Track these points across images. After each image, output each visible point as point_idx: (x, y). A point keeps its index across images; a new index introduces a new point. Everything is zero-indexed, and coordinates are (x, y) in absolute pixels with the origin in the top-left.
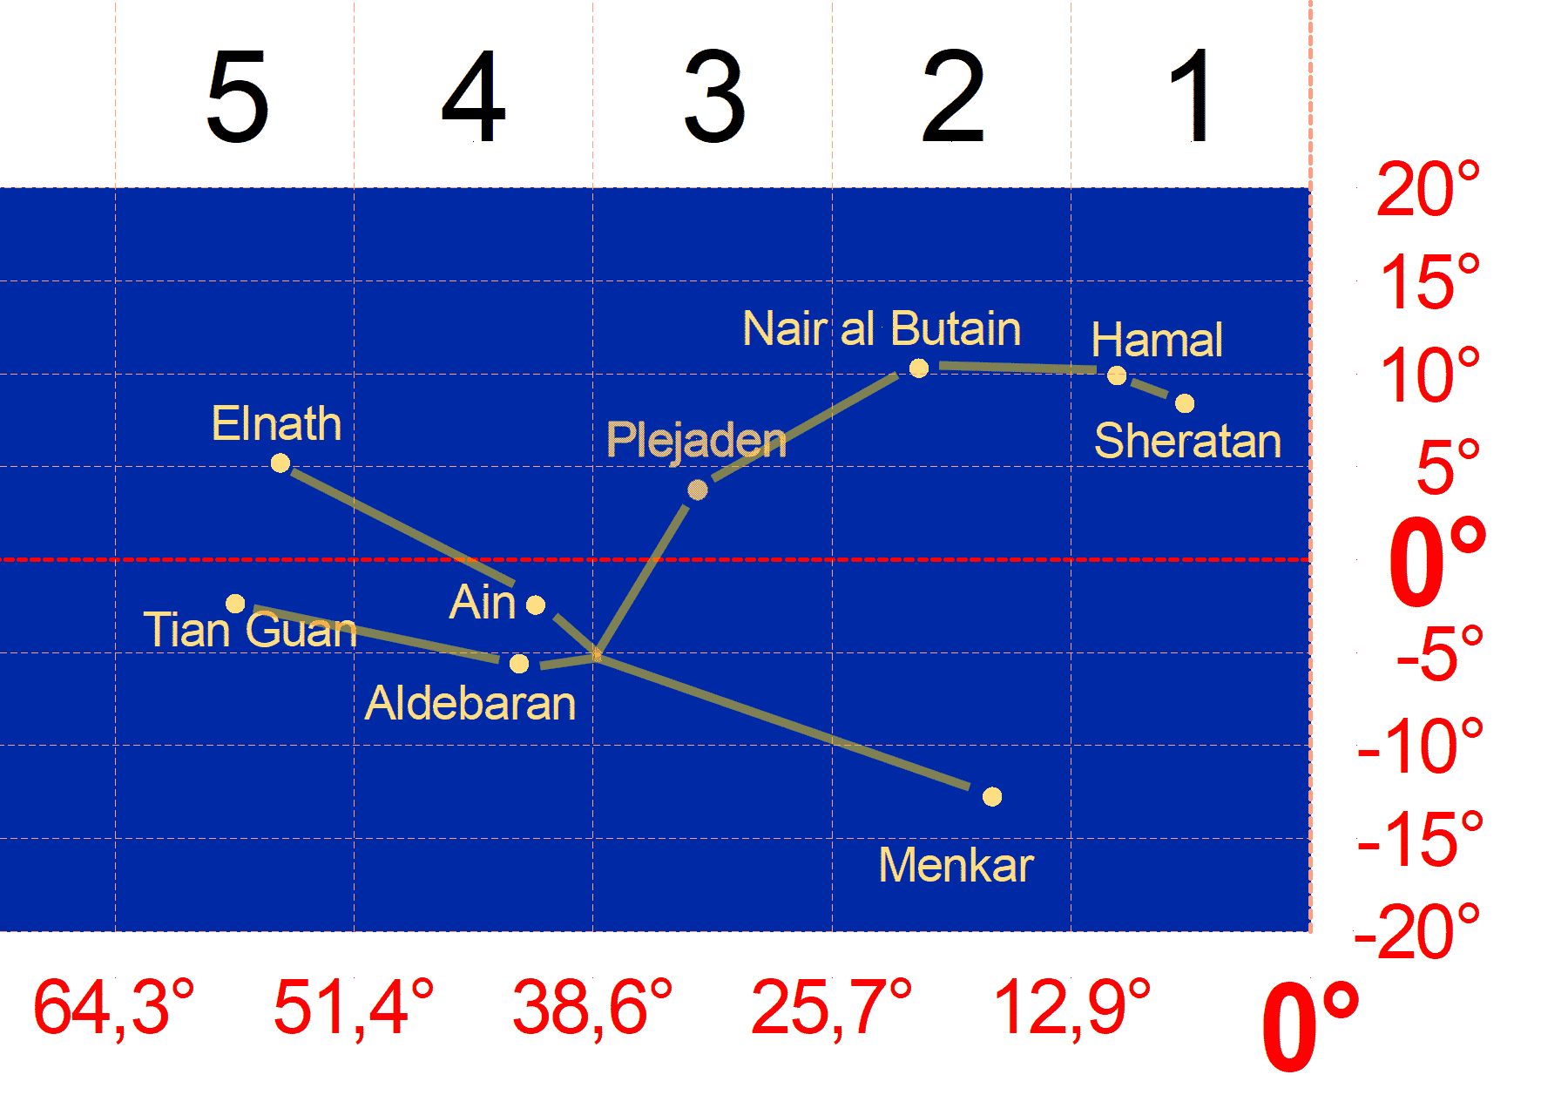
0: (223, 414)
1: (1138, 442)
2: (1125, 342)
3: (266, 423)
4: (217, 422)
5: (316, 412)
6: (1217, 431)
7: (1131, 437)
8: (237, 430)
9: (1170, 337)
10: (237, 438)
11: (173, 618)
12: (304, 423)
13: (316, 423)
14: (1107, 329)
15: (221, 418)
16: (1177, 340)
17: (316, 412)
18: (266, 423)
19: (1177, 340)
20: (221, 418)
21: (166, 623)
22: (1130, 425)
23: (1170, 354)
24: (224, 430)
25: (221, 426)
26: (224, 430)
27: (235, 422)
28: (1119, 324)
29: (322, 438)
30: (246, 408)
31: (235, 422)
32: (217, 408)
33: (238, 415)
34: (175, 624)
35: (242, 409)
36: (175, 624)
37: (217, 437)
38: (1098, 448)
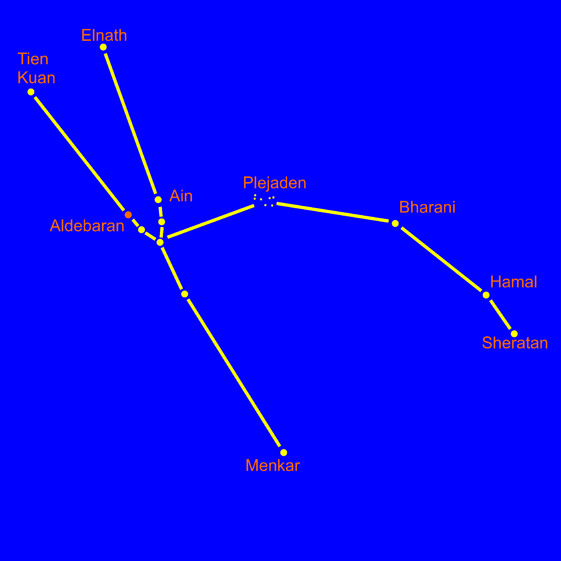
0: (85, 32)
1: (497, 343)
2: (502, 282)
3: (100, 35)
4: (83, 35)
5: (118, 31)
6: (525, 339)
7: (495, 341)
8: (91, 37)
9: (518, 281)
10: (90, 40)
11: (27, 55)
12: (114, 35)
13: (118, 35)
14: (496, 278)
15: (85, 33)
16: (520, 282)
17: (118, 31)
18: (100, 35)
19: (520, 282)
20: (85, 33)
21: (25, 56)
22: (494, 337)
23: (518, 286)
24: (85, 38)
25: (85, 36)
26: (85, 38)
27: (89, 35)
28: (500, 276)
29: (120, 40)
30: (94, 30)
31: (89, 35)
32: (83, 30)
33: (91, 32)
34: (29, 57)
35: (92, 31)
36: (29, 57)
37: (83, 40)
38: (483, 345)
